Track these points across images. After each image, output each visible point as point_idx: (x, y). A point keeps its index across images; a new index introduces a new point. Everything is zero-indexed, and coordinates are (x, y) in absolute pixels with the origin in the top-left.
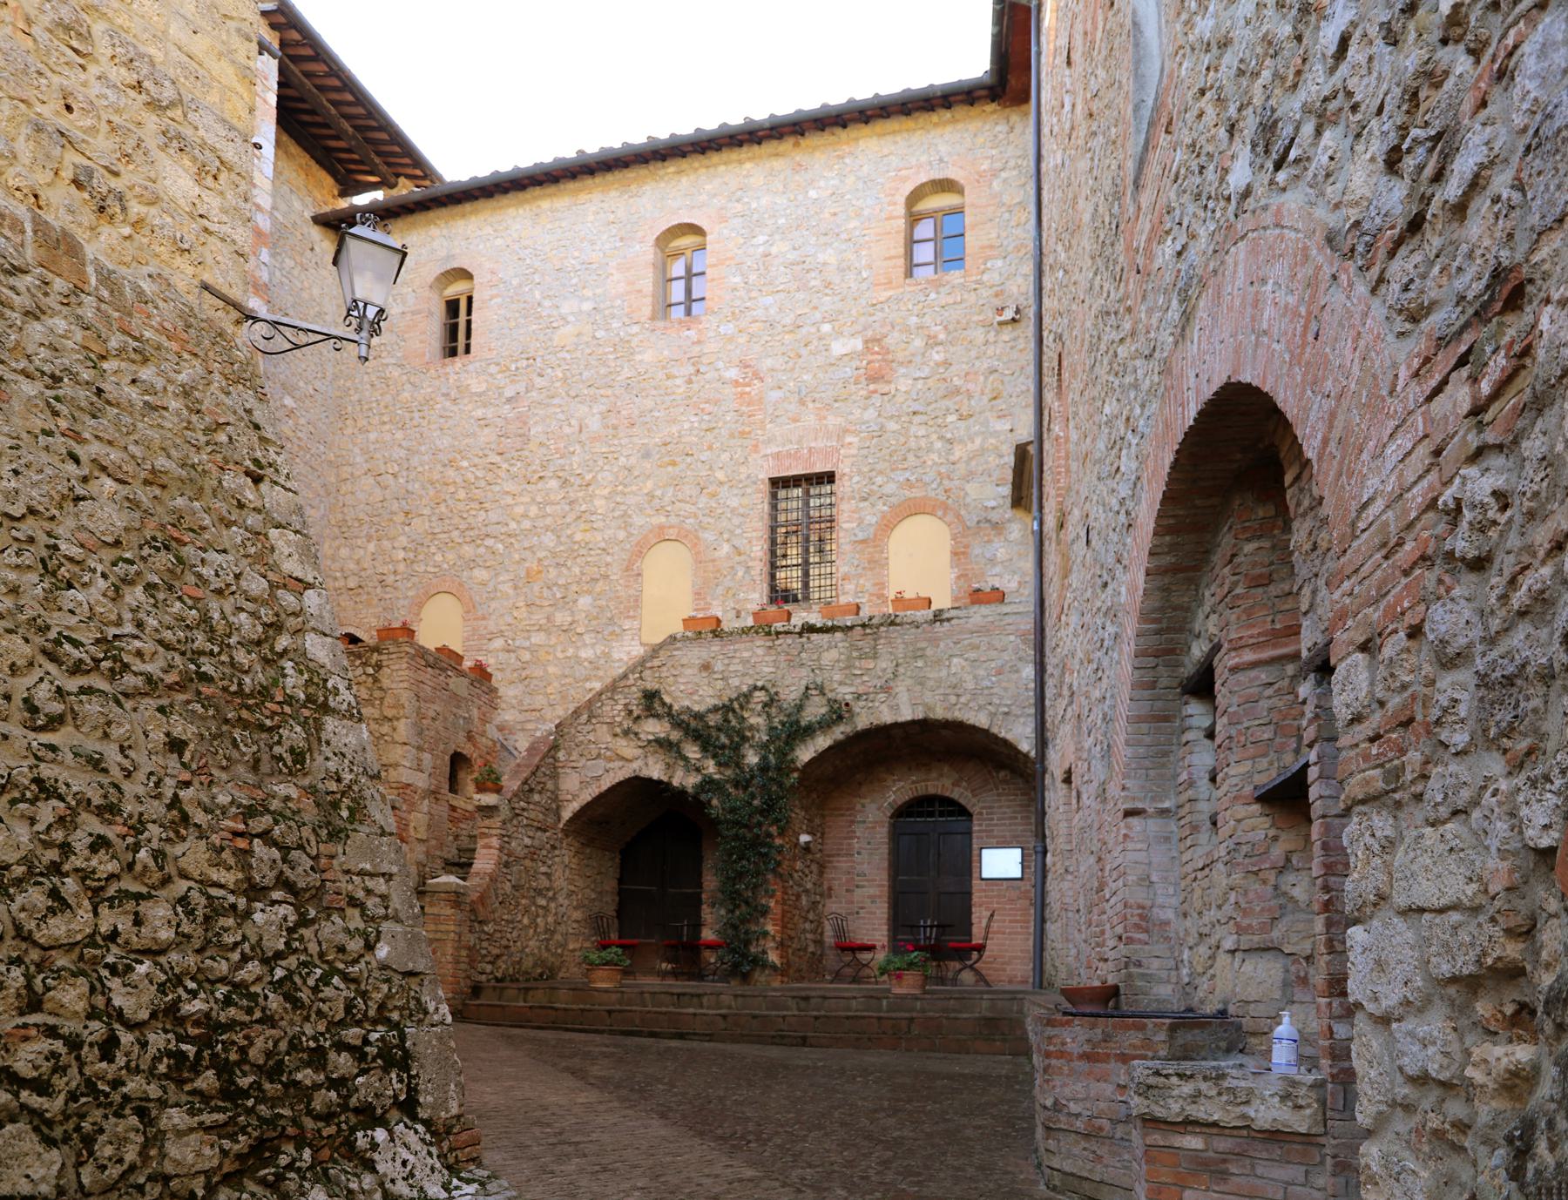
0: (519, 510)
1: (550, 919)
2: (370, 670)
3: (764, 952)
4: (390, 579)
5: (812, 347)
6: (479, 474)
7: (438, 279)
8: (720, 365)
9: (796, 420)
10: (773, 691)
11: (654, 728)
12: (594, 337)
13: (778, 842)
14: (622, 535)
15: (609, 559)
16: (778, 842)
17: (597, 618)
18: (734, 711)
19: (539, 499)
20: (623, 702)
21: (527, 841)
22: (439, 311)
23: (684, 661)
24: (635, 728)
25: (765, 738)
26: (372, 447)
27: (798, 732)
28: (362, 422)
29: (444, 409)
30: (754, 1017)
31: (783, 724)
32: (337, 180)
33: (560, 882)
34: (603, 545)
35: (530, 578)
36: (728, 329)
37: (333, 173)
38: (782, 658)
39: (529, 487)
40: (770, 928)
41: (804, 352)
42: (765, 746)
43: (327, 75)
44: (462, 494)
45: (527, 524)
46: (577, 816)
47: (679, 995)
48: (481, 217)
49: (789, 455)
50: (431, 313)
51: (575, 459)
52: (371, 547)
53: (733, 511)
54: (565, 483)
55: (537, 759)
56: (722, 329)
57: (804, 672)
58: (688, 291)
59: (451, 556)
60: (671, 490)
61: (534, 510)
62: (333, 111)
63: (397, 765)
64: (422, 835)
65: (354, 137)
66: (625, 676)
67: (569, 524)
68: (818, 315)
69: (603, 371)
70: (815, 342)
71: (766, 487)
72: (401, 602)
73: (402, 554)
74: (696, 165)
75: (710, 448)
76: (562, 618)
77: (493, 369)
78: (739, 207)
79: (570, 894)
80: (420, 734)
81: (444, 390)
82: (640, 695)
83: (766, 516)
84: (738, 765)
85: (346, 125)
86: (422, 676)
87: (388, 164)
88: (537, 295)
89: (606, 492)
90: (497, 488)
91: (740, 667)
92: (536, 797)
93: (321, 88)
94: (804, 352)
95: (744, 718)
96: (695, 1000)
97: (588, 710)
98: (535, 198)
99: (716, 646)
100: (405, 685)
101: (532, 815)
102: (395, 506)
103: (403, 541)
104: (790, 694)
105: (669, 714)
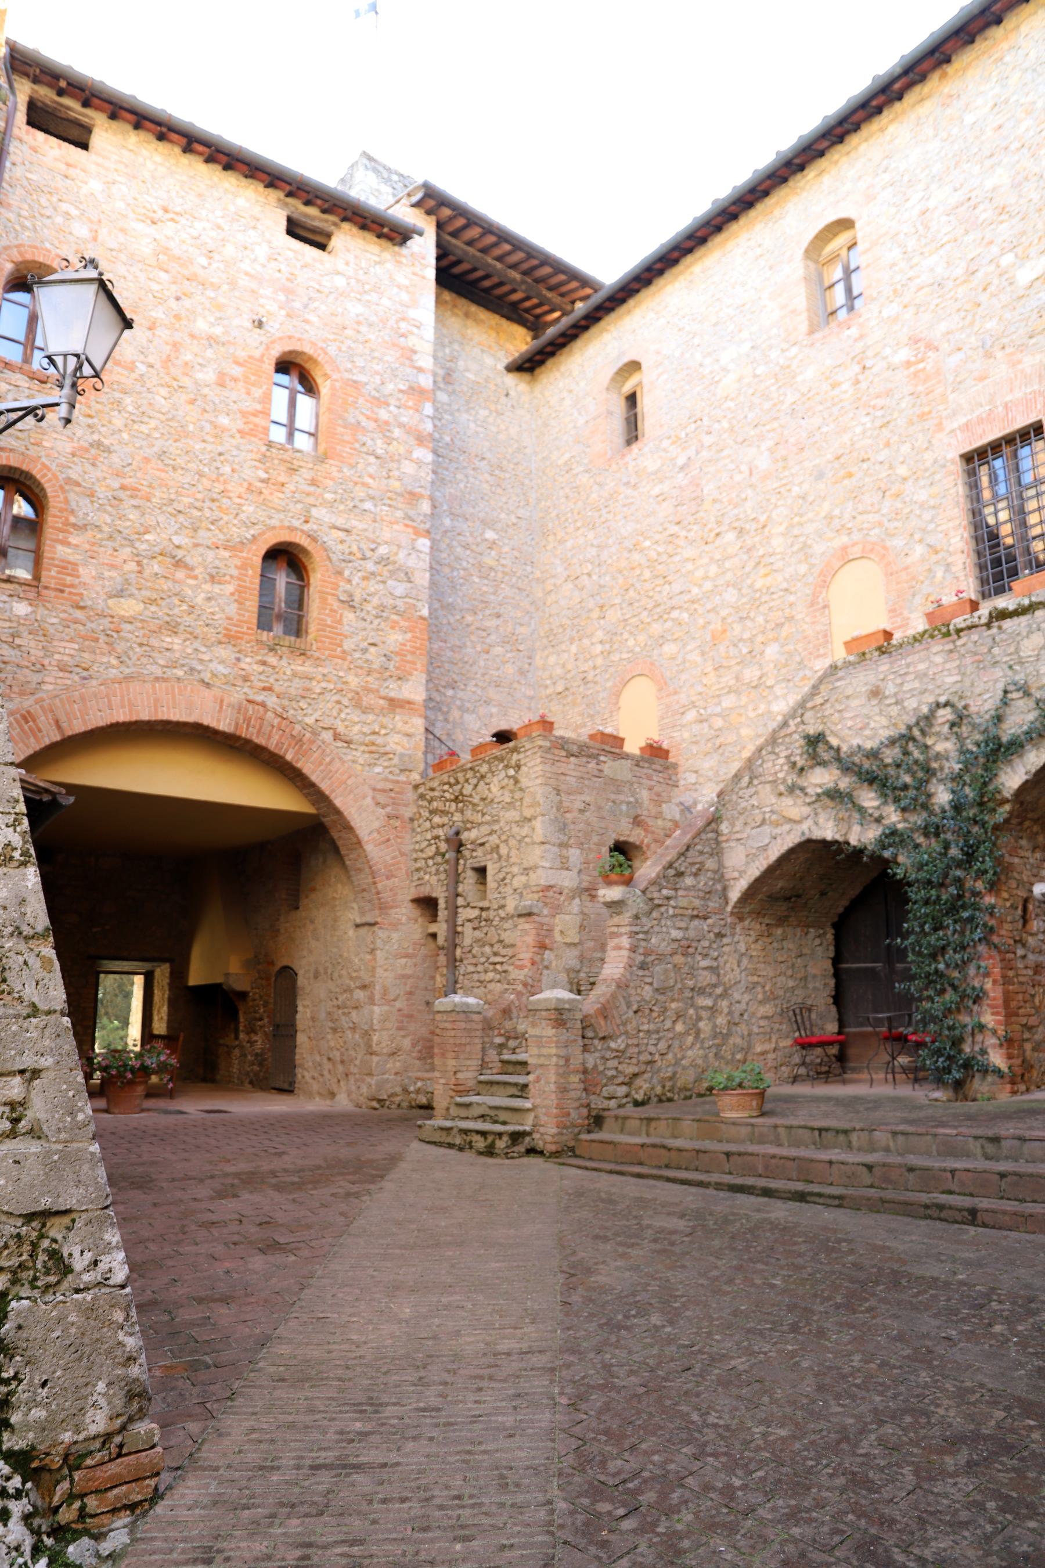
0: (699, 574)
1: (721, 1020)
2: (512, 772)
3: (984, 1052)
4: (590, 676)
5: (992, 289)
6: (661, 549)
7: (613, 380)
8: (888, 351)
9: (982, 379)
10: (960, 705)
11: (822, 778)
12: (755, 376)
13: (989, 900)
14: (803, 569)
15: (792, 598)
16: (989, 900)
17: (786, 665)
18: (914, 739)
19: (718, 557)
20: (784, 754)
21: (675, 934)
22: (619, 407)
23: (849, 691)
24: (802, 782)
25: (957, 767)
26: (569, 554)
27: (1000, 751)
28: (561, 534)
29: (627, 497)
30: (911, 1170)
31: (978, 745)
32: (529, 328)
33: (733, 971)
34: (785, 585)
35: (716, 639)
36: (892, 309)
37: (522, 322)
38: (968, 660)
39: (707, 548)
40: (989, 1019)
41: (983, 298)
42: (957, 778)
43: (483, 235)
44: (647, 574)
45: (708, 586)
46: (749, 895)
47: (820, 1130)
48: (644, 306)
49: (980, 420)
50: (610, 413)
51: (749, 504)
52: (574, 649)
53: (922, 506)
54: (741, 531)
55: (689, 836)
56: (885, 314)
57: (998, 672)
58: (849, 290)
59: (642, 638)
60: (851, 503)
61: (713, 570)
62: (499, 265)
63: (534, 868)
64: (573, 937)
65: (523, 282)
66: (785, 724)
67: (748, 574)
68: (995, 250)
69: (767, 405)
70: (996, 282)
71: (958, 467)
72: (602, 695)
73: (599, 648)
74: (836, 157)
75: (887, 445)
76: (750, 674)
77: (666, 443)
78: (886, 177)
79: (750, 988)
80: (563, 828)
81: (625, 480)
82: (802, 742)
83: (962, 500)
84: (925, 806)
85: (515, 275)
86: (562, 767)
87: (562, 295)
88: (698, 357)
89: (782, 529)
90: (677, 558)
91: (916, 684)
92: (689, 881)
93: (484, 251)
94: (983, 298)
95: (927, 747)
96: (842, 1138)
97: (751, 770)
98: (688, 267)
99: (884, 665)
100: (539, 781)
101: (683, 902)
102: (591, 604)
103: (600, 634)
104: (983, 704)
105: (838, 759)
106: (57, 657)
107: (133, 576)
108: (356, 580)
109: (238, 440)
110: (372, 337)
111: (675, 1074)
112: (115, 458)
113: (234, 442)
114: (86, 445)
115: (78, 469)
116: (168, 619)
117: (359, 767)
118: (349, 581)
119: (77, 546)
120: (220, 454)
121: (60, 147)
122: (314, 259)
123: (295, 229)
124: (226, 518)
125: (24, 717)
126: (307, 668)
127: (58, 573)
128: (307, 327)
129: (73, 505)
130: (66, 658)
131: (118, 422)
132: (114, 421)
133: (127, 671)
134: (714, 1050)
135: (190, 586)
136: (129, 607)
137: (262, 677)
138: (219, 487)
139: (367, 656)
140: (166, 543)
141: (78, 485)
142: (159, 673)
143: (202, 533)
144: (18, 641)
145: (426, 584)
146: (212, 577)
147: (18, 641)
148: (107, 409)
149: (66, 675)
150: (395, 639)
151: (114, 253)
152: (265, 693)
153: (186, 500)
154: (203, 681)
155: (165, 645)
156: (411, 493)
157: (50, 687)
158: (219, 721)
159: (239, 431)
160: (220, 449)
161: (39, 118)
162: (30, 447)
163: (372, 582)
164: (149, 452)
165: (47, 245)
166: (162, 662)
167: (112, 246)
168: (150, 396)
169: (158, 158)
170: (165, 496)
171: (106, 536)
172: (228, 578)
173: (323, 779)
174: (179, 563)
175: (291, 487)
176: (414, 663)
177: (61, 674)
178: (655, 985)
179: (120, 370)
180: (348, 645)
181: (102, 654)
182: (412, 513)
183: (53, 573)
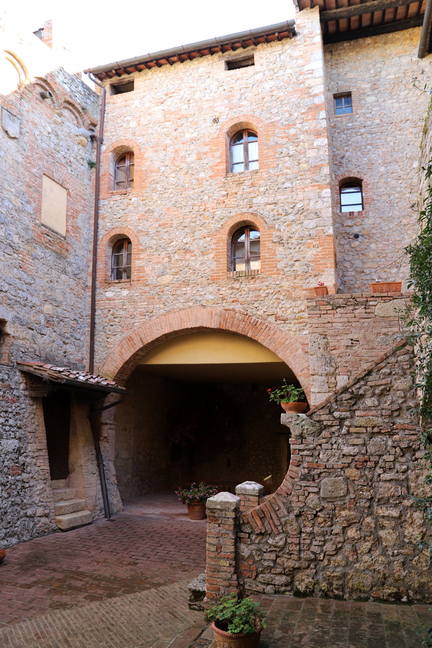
80: (330, 362)
106: (139, 310)
107: (167, 264)
108: (282, 228)
109: (211, 181)
110: (282, 94)
111: (344, 575)
112: (156, 214)
113: (208, 183)
114: (143, 213)
115: (141, 225)
116: (184, 279)
117: (292, 333)
118: (279, 230)
119: (143, 258)
120: (202, 192)
121: (122, 96)
122: (242, 74)
123: (231, 65)
124: (207, 221)
125: (129, 339)
126: (257, 284)
127: (137, 273)
128: (242, 109)
129: (141, 241)
130: (143, 310)
131: (155, 197)
132: (154, 197)
133: (167, 309)
134: (401, 559)
135: (192, 260)
136: (167, 279)
137: (232, 296)
138: (203, 208)
139: (294, 268)
140: (181, 243)
141: (142, 231)
142: (182, 306)
143: (196, 233)
144: (125, 307)
145: (330, 214)
146: (203, 252)
147: (125, 307)
148: (150, 194)
149: (143, 317)
150: (310, 253)
151: (147, 126)
152: (234, 304)
153: (188, 220)
154: (202, 305)
155: (183, 292)
156: (315, 166)
157: (137, 324)
158: (211, 323)
159: (210, 177)
160: (201, 189)
161: (118, 89)
162: (123, 223)
163: (294, 225)
164: (169, 205)
165: (122, 138)
166: (182, 301)
167: (145, 124)
168: (167, 179)
169: (161, 75)
170: (178, 222)
171: (155, 250)
172: (210, 250)
173: (270, 344)
174: (187, 251)
175: (240, 193)
176: (325, 264)
177: (141, 317)
178: (322, 494)
179: (153, 174)
180: (280, 265)
181: (157, 304)
182: (316, 178)
183: (135, 274)
